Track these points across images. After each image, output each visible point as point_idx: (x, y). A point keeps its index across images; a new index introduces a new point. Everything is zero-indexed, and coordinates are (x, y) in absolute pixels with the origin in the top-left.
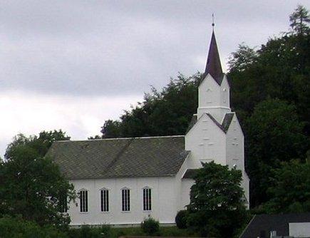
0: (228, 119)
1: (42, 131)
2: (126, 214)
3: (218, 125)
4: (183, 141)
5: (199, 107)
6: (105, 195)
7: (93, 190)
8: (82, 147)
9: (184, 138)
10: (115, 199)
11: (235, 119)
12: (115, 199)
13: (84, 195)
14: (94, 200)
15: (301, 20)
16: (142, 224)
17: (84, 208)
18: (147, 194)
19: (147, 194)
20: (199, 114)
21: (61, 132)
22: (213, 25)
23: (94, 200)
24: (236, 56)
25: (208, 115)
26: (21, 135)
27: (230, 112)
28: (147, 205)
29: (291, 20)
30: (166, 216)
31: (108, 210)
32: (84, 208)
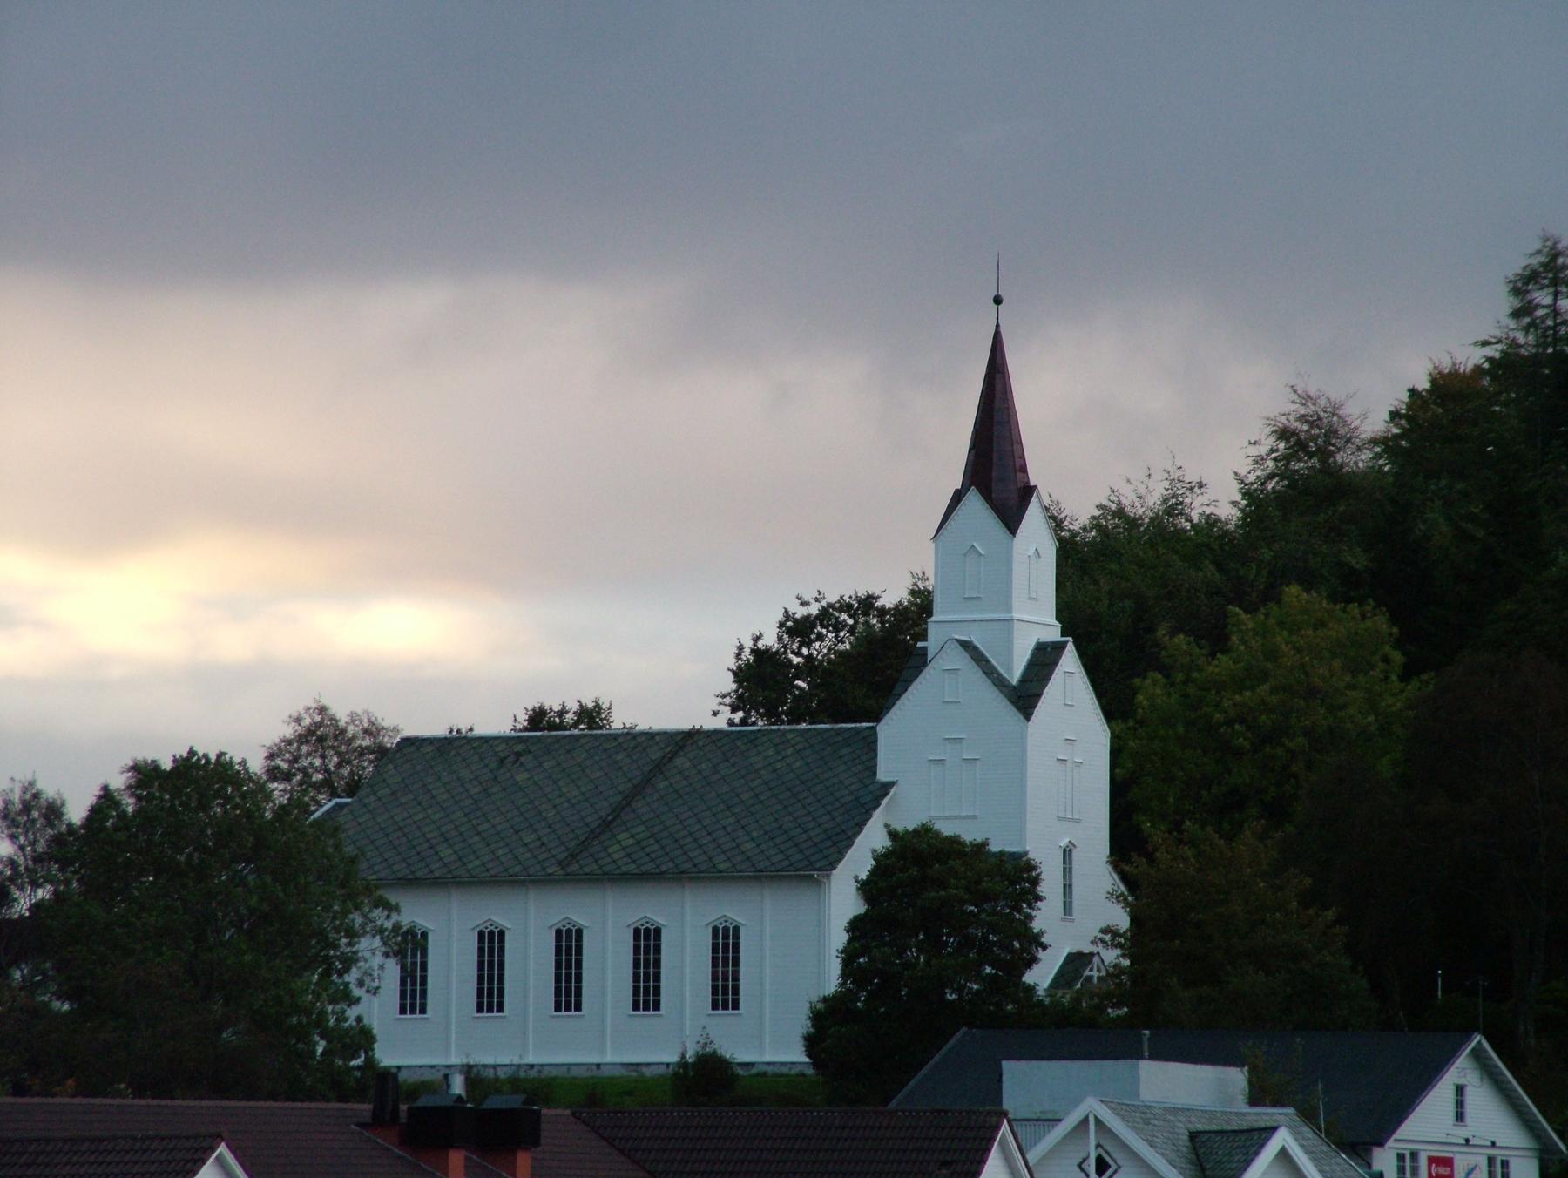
0: (1045, 658)
1: (533, 703)
2: (646, 1019)
3: (999, 681)
4: (869, 744)
5: (934, 618)
6: (569, 946)
7: (450, 926)
8: (502, 761)
9: (874, 728)
10: (608, 967)
11: (1070, 661)
12: (608, 967)
13: (410, 949)
14: (452, 968)
15: (1556, 295)
16: (683, 1064)
17: (413, 999)
18: (726, 945)
19: (726, 945)
20: (932, 643)
21: (598, 706)
22: (998, 300)
23: (452, 968)
24: (1283, 434)
25: (966, 646)
26: (322, 710)
27: (1053, 634)
28: (725, 994)
29: (1517, 291)
30: (769, 1035)
31: (423, 1011)
32: (413, 999)
